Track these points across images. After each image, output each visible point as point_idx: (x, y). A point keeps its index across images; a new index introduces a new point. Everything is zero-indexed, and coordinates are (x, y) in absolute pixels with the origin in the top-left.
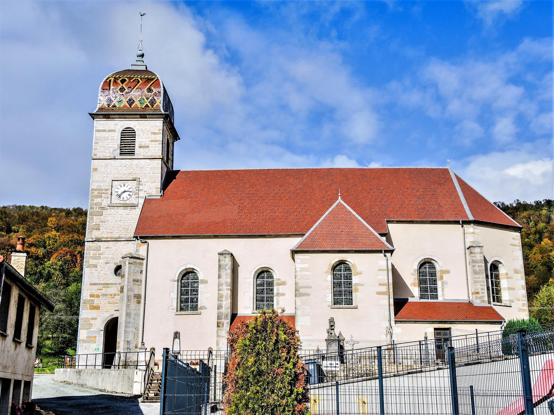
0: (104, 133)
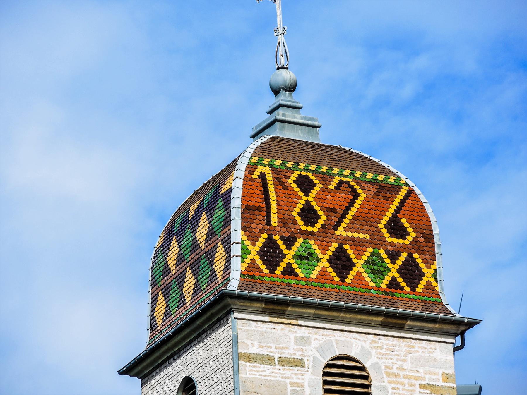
0: (268, 369)
